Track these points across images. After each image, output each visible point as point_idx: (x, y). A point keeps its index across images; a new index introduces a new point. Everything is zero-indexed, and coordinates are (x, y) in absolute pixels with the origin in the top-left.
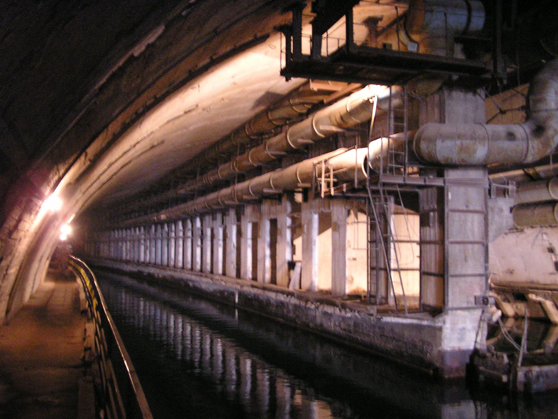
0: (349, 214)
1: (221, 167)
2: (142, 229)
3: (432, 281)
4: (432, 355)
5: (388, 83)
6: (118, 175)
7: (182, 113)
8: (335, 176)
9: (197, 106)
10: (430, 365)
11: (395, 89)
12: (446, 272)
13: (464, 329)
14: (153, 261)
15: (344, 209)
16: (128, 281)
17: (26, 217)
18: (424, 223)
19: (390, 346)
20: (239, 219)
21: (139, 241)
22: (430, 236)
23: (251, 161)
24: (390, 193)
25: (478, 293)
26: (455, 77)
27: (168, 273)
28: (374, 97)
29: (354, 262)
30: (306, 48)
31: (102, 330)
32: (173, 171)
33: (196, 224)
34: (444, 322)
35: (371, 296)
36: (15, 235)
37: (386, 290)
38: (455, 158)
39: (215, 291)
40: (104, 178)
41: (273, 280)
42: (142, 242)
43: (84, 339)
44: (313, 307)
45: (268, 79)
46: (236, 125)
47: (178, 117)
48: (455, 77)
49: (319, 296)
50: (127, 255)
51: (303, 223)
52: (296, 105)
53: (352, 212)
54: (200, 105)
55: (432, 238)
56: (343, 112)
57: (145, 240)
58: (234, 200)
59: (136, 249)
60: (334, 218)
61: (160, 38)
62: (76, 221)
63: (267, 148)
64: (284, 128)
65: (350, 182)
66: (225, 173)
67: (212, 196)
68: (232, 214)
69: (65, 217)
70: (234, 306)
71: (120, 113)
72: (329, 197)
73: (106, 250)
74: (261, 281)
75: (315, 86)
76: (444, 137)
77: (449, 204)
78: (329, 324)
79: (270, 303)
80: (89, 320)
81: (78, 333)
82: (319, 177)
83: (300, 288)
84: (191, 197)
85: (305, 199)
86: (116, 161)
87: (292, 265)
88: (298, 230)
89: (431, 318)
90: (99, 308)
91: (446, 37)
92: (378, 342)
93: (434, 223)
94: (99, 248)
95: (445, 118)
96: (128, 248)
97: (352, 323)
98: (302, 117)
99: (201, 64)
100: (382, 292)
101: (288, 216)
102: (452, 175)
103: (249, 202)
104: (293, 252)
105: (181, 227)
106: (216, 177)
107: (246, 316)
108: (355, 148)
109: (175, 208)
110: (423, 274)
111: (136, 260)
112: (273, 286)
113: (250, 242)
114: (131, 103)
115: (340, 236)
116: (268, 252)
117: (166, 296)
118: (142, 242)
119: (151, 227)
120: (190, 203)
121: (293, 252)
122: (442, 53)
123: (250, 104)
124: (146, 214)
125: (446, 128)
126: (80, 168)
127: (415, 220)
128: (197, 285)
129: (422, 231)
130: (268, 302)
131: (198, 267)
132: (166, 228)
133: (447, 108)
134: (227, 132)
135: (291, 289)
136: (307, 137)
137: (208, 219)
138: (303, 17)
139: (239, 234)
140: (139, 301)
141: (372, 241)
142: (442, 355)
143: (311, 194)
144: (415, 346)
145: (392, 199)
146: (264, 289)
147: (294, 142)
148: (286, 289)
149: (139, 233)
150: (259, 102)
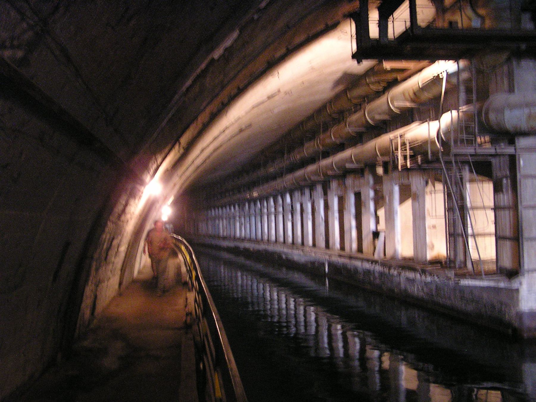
0: (427, 183)
1: (306, 145)
2: (237, 207)
3: (508, 245)
4: (510, 315)
5: (455, 57)
6: (211, 158)
7: (265, 98)
8: (411, 149)
9: (279, 91)
10: (509, 325)
11: (462, 63)
12: (520, 236)
14: (248, 236)
15: (422, 179)
16: (226, 255)
17: (132, 202)
18: (497, 189)
19: (470, 308)
20: (325, 194)
21: (234, 218)
22: (504, 201)
23: (333, 138)
24: (464, 163)
26: (523, 46)
27: (257, 247)
28: (444, 72)
29: (433, 231)
30: (374, 31)
31: (200, 296)
32: (262, 152)
33: (286, 200)
34: (521, 284)
35: (450, 261)
36: (123, 218)
37: (235, 231)
38: (524, 126)
39: (306, 262)
40: (198, 162)
41: (360, 249)
42: (238, 218)
43: (186, 307)
44: (395, 273)
45: (344, 61)
46: (318, 105)
47: (262, 103)
48: (523, 46)
49: (403, 263)
50: (223, 231)
51: (385, 194)
52: (373, 83)
53: (430, 182)
54: (281, 90)
55: (506, 204)
56: (416, 88)
57: (240, 217)
58: (319, 175)
59: (232, 227)
60: (414, 188)
61: (236, 41)
62: (175, 203)
63: (347, 126)
64: (363, 106)
65: (425, 154)
66: (311, 150)
67: (299, 173)
68: (319, 189)
69: (166, 198)
70: (324, 275)
71: (207, 105)
72: (405, 168)
73: (205, 228)
74: (348, 250)
75: (388, 65)
76: (512, 107)
77: (522, 170)
78: (413, 288)
79: (358, 272)
80: (190, 290)
81: (181, 301)
82: (395, 150)
83: (385, 254)
84: (280, 174)
85: (386, 171)
86: (208, 146)
87: (376, 234)
88: (381, 202)
89: (508, 280)
90: (197, 278)
91: (511, 9)
92: (459, 304)
93: (507, 190)
94: (198, 225)
95: (514, 87)
96: (225, 225)
97: (434, 287)
98: (379, 94)
99: (278, 54)
100: (461, 257)
101: (371, 188)
102: (522, 142)
103: (335, 177)
104: (377, 222)
106: (302, 155)
107: (336, 285)
108: (427, 121)
109: (266, 186)
110: (499, 238)
111: (232, 236)
112: (360, 255)
113: (336, 215)
114: (217, 95)
115: (419, 205)
116: (354, 223)
117: (260, 267)
118: (238, 218)
119: (244, 205)
120: (279, 181)
121: (377, 222)
122: (507, 26)
123: (329, 85)
124: (239, 192)
125: (514, 98)
126: (175, 156)
127: (488, 187)
128: (290, 257)
129: (496, 197)
130: (356, 270)
131: (290, 240)
133: (516, 78)
134: (310, 112)
135: (376, 257)
136: (384, 113)
137: (297, 194)
139: (327, 207)
140: (236, 274)
141: (449, 209)
142: (520, 315)
143: (390, 167)
144: (493, 307)
145: (467, 168)
146: (351, 258)
147: (373, 119)
148: (371, 257)
149: (234, 210)
150: (338, 82)
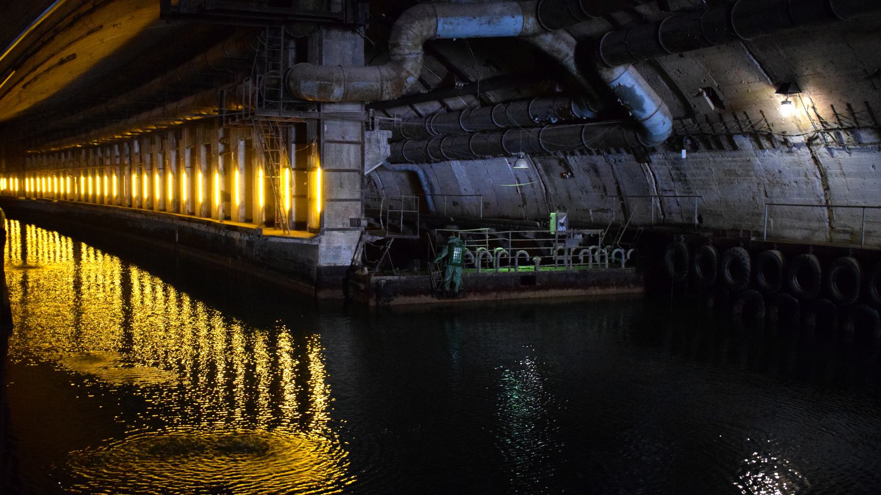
13: (340, 247)
25: (354, 216)
33: (134, 149)
34: (320, 241)
105: (117, 153)
132: (100, 154)
137: (146, 141)
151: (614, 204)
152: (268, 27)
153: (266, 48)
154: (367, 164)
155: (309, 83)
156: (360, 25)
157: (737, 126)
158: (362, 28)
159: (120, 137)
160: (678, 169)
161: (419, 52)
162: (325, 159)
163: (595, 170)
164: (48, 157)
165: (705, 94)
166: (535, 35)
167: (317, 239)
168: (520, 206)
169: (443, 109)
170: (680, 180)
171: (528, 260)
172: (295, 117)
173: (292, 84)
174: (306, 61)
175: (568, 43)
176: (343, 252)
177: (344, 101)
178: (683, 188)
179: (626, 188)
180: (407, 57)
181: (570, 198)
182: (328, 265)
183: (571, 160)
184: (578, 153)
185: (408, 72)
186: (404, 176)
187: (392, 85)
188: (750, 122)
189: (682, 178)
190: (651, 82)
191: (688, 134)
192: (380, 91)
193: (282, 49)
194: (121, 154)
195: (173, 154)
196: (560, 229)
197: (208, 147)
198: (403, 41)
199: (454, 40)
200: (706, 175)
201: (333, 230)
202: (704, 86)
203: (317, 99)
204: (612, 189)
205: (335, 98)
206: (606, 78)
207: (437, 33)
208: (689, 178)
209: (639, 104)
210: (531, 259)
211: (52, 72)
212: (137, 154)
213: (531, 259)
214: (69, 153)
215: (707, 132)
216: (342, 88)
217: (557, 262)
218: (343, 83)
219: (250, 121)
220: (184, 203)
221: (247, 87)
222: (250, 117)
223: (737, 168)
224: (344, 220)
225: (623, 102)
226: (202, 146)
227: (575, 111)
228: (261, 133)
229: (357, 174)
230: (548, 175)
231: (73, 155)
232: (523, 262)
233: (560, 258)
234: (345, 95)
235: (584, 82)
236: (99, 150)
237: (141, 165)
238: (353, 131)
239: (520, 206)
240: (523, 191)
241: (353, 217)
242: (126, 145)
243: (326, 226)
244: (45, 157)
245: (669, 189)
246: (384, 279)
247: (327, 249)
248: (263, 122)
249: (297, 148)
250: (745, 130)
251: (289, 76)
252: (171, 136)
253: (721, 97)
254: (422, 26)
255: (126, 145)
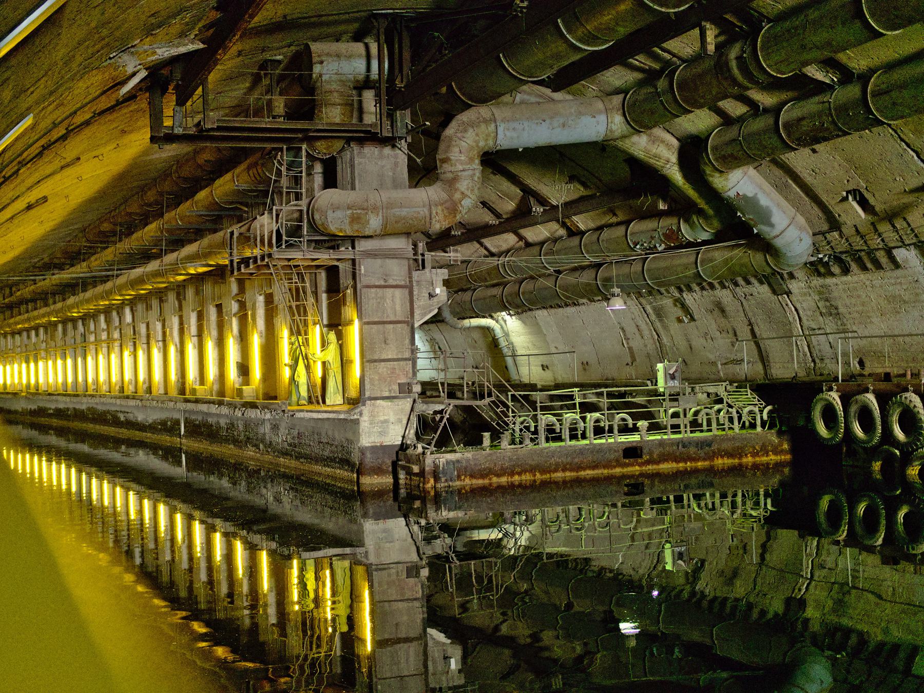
13: (386, 421)
25: (403, 380)
33: (125, 318)
34: (361, 414)
93: (350, 302)
105: (103, 325)
137: (140, 307)
138: (164, 118)
151: (746, 350)
152: (285, 147)
153: (284, 173)
154: (417, 312)
155: (339, 214)
156: (401, 138)
157: (897, 237)
158: (403, 143)
159: (107, 303)
160: (827, 300)
161: (476, 167)
162: (363, 309)
163: (721, 309)
164: (13, 337)
165: (850, 198)
166: (624, 137)
167: (357, 411)
168: (627, 364)
169: (520, 242)
170: (831, 314)
171: (631, 426)
172: (325, 257)
173: (317, 217)
174: (334, 186)
175: (668, 146)
176: (392, 427)
177: (385, 234)
178: (836, 323)
179: (763, 330)
180: (459, 174)
181: (691, 348)
182: (373, 444)
183: (688, 298)
184: (697, 288)
185: (463, 193)
186: (476, 335)
187: (443, 210)
188: (912, 230)
189: (833, 312)
190: (779, 188)
191: (835, 252)
192: (428, 219)
193: (304, 174)
194: (108, 326)
195: (175, 321)
196: (671, 383)
197: (219, 307)
198: (454, 154)
199: (520, 150)
200: (863, 304)
201: (376, 399)
202: (850, 188)
203: (349, 233)
204: (744, 332)
205: (371, 231)
206: (720, 186)
207: (498, 142)
208: (842, 310)
209: (765, 217)
210: (635, 425)
211: (16, 221)
212: (128, 324)
213: (635, 425)
214: (41, 330)
215: (857, 248)
216: (380, 217)
217: (669, 427)
218: (381, 211)
219: (267, 266)
220: (191, 383)
221: (262, 226)
222: (266, 260)
223: (902, 293)
224: (390, 385)
225: (744, 216)
226: (211, 306)
227: (686, 232)
228: (281, 279)
229: (404, 325)
230: (661, 321)
231: (46, 332)
232: (625, 429)
233: (675, 421)
234: (385, 225)
235: (691, 193)
236: (80, 323)
237: (135, 339)
238: (397, 270)
239: (627, 364)
240: (631, 344)
241: (402, 381)
242: (114, 313)
243: (367, 394)
244: (9, 337)
245: (818, 327)
246: (444, 458)
247: (371, 424)
248: (283, 267)
249: (329, 298)
250: (907, 242)
251: (314, 207)
252: (171, 297)
253: (872, 201)
254: (477, 135)
255: (114, 313)
